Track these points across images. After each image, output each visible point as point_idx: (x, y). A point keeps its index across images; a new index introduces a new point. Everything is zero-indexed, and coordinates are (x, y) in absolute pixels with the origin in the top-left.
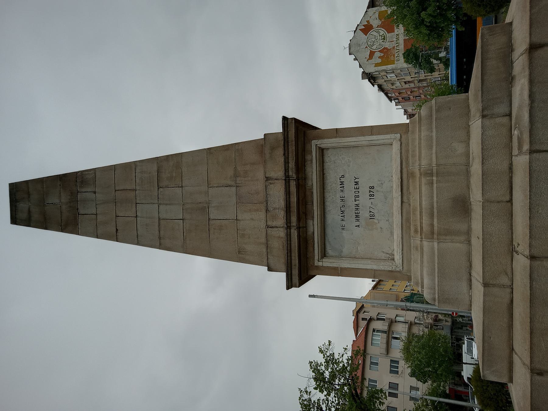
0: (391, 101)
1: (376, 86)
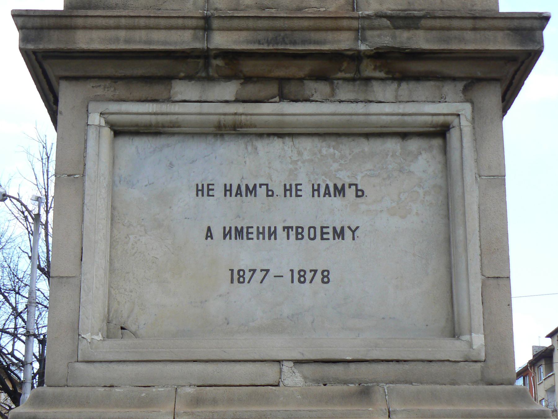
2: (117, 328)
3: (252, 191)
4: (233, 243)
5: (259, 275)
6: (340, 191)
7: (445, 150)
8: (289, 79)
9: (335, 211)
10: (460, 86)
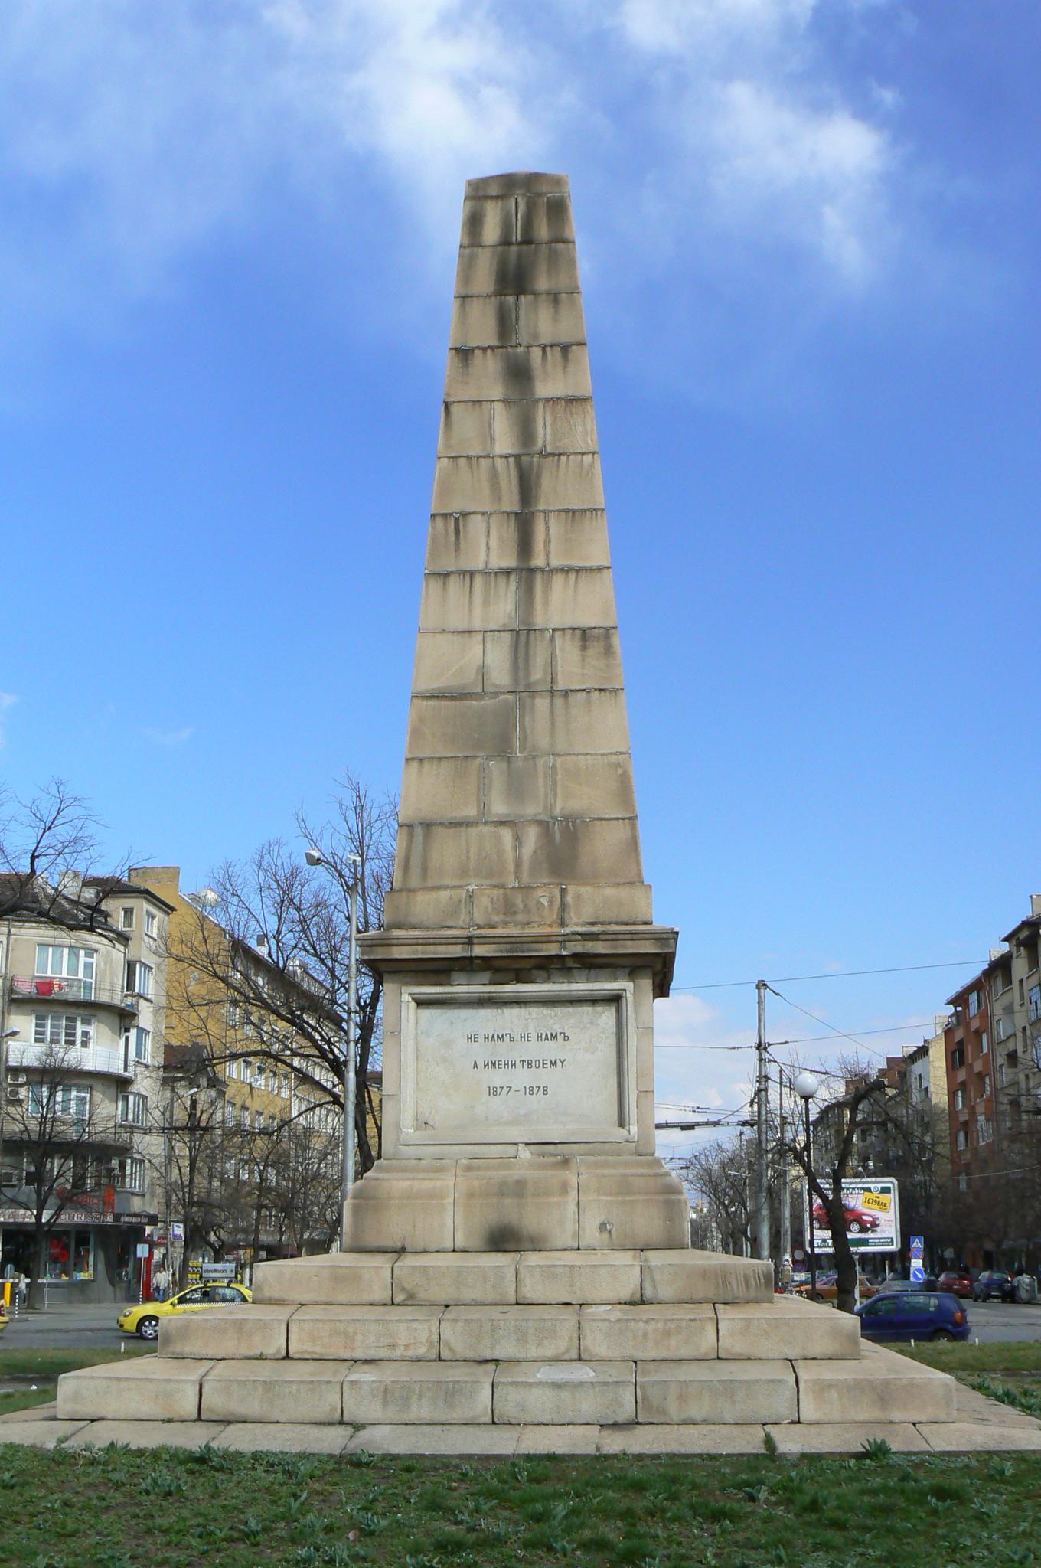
0: (954, 1002)
1: (1006, 947)
2: (423, 1124)
3: (501, 1038)
4: (489, 1071)
5: (505, 1090)
6: (554, 1037)
7: (618, 1011)
8: (521, 969)
9: (552, 1051)
10: (627, 971)
